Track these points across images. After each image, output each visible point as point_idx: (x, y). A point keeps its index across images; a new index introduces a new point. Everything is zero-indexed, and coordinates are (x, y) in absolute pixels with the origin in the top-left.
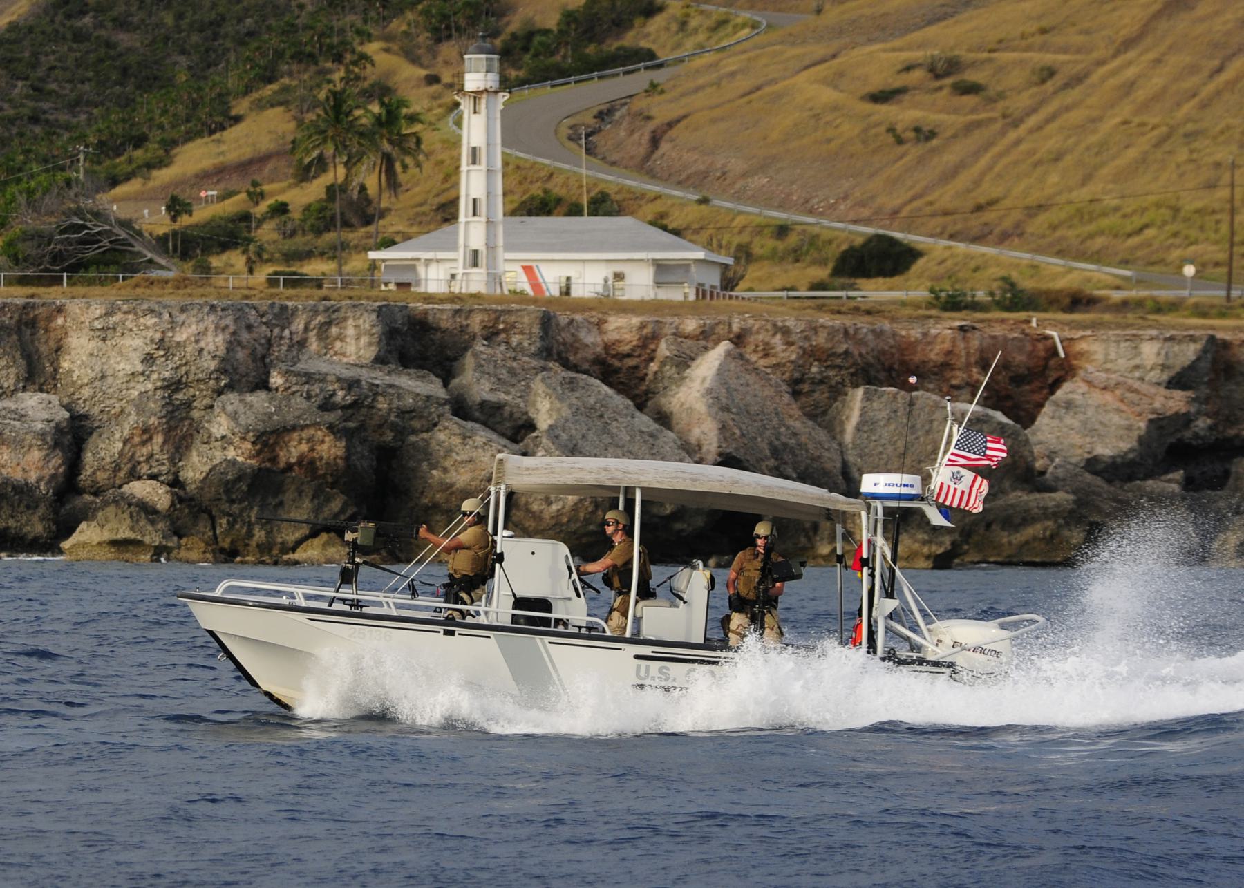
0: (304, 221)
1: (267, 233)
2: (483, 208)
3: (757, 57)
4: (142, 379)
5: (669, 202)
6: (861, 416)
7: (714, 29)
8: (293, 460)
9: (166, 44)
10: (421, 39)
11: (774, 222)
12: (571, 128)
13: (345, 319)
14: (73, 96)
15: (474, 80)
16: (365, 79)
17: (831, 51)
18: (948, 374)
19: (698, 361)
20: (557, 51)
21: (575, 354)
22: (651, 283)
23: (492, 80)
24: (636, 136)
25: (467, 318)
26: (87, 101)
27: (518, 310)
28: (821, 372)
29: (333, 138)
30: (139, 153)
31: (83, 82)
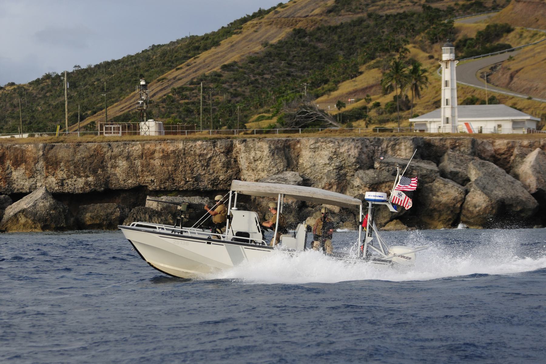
0: (386, 109)
2: (450, 102)
10: (427, 43)
13: (401, 143)
14: (302, 66)
15: (446, 56)
16: (407, 57)
19: (528, 155)
24: (505, 76)
30: (326, 86)
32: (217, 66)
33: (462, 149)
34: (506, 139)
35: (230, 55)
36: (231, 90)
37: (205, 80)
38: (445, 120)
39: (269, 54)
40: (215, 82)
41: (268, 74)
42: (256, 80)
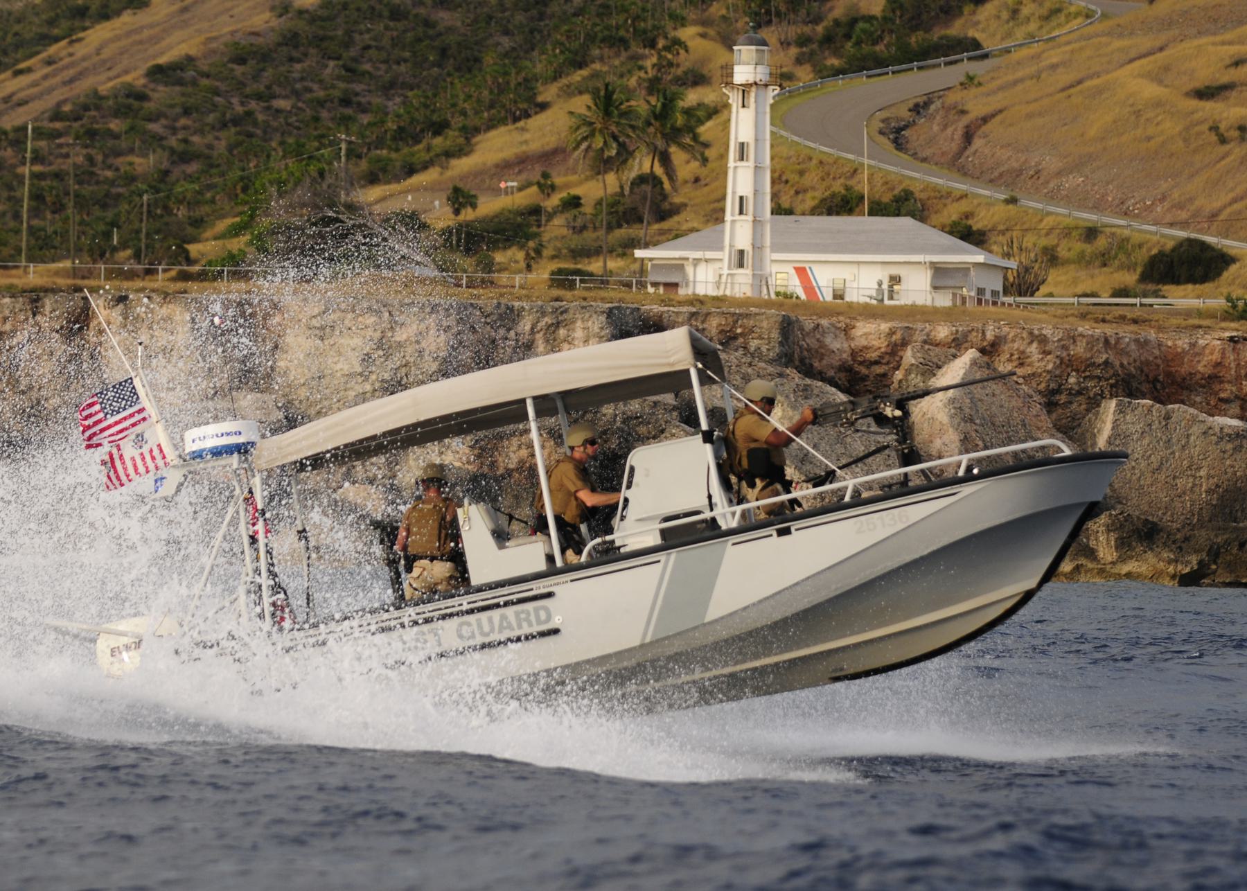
0: (595, 215)
1: (556, 229)
2: (750, 206)
3: (1081, 49)
4: (360, 379)
5: (975, 202)
6: (1113, 429)
7: (1047, 18)
8: (511, 466)
9: (488, 23)
10: (740, 25)
11: (1082, 224)
12: (883, 121)
13: (574, 322)
14: (387, 77)
15: (743, 73)
16: (678, 65)
17: (1158, 44)
18: (1217, 387)
19: (944, 369)
20: (881, 38)
21: (821, 360)
22: (929, 288)
23: (761, 74)
24: (949, 131)
25: (703, 322)
26: (403, 83)
27: (756, 314)
28: (1079, 383)
29: (601, 131)
30: (438, 141)
31: (398, 63)
32: (135, 69)
33: (753, 344)
34: (886, 321)
35: (177, 35)
36: (173, 142)
37: (98, 108)
38: (735, 258)
39: (291, 39)
40: (126, 115)
41: (286, 97)
42: (249, 114)
